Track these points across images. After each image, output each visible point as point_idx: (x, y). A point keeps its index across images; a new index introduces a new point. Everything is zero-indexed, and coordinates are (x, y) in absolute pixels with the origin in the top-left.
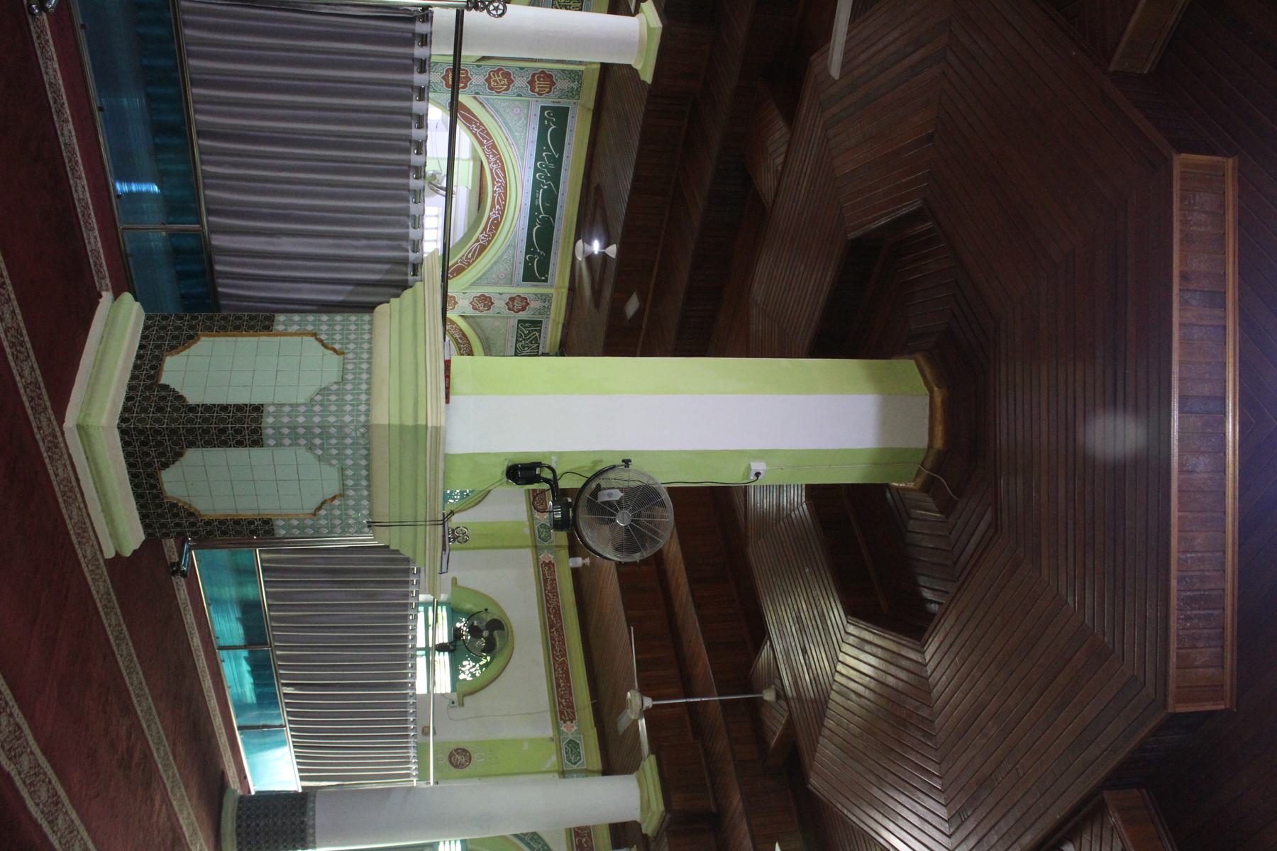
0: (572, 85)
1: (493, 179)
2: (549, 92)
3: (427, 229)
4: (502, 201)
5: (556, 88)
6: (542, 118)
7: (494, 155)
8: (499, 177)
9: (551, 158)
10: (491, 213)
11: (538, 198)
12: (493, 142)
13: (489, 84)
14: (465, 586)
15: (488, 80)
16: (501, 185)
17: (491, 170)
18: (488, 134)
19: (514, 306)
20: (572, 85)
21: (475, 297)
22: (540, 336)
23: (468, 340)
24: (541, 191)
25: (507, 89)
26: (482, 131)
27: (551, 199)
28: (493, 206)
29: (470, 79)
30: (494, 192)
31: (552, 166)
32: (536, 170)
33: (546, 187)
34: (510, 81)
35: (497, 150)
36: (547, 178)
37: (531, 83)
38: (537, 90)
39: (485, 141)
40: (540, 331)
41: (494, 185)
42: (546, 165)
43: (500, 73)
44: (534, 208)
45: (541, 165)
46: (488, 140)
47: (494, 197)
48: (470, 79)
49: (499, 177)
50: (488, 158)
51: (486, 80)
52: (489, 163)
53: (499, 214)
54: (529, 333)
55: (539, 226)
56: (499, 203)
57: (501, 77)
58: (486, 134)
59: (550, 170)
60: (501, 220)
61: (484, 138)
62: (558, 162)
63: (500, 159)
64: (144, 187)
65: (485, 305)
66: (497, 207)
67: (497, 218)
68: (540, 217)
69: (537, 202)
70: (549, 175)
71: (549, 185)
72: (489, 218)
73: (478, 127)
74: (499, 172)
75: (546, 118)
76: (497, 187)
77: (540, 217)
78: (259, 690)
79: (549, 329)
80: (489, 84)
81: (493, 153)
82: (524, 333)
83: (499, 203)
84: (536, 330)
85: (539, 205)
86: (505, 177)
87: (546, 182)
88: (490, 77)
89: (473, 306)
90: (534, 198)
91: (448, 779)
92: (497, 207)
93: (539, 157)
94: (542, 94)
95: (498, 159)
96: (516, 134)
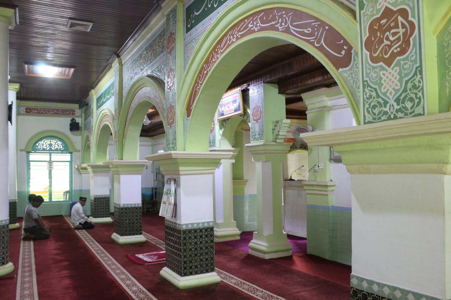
1: (229, 46)
30: (237, 39)
39: (205, 72)
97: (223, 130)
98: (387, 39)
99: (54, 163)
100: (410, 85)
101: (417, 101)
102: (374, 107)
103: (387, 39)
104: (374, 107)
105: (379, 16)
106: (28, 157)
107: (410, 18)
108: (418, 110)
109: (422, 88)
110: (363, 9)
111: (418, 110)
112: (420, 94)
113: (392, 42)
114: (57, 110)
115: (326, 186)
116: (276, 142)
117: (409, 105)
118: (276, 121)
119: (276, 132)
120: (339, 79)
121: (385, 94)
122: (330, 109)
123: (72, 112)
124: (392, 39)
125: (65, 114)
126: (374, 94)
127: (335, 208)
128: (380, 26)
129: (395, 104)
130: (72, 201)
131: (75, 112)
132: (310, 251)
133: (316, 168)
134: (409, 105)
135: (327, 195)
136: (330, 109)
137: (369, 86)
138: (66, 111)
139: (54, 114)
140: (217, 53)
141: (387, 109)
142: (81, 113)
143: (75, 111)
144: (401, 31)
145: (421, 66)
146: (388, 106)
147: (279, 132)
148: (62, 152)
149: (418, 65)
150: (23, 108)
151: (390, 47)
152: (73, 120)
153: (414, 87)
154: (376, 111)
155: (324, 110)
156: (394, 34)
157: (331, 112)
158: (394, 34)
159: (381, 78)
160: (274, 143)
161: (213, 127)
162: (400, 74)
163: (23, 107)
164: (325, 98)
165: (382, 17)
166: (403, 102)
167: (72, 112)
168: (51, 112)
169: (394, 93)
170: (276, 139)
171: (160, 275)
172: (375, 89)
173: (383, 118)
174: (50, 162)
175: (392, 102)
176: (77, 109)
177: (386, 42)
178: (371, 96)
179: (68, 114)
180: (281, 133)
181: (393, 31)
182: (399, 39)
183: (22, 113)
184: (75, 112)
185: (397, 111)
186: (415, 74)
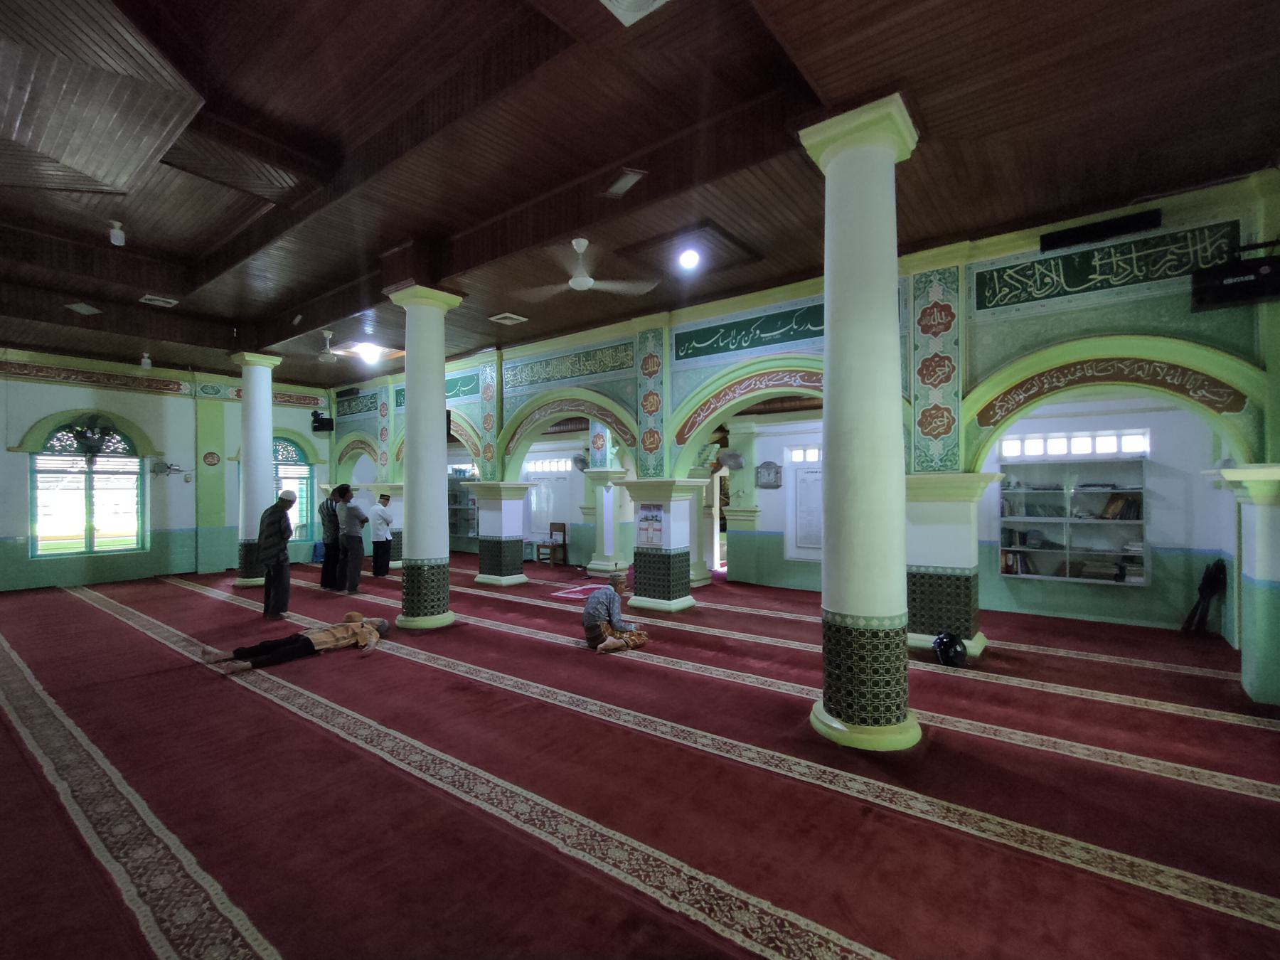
0: (650, 339)
1: (752, 390)
2: (657, 357)
3: (90, 534)
4: (778, 375)
5: (654, 352)
6: (687, 356)
7: (726, 394)
8: (750, 384)
9: (724, 337)
10: (795, 385)
11: (772, 336)
12: (712, 397)
13: (653, 411)
14: (216, 571)
15: (651, 413)
16: (759, 380)
17: (742, 394)
18: (704, 404)
19: (939, 324)
20: (650, 339)
21: (923, 382)
22: (1011, 268)
23: (1033, 378)
24: (762, 336)
25: (657, 395)
26: (702, 410)
27: (770, 323)
28: (786, 385)
29: (651, 429)
30: (767, 386)
31: (734, 333)
32: (740, 347)
33: (758, 332)
34: (651, 394)
35: (721, 392)
36: (747, 335)
37: (650, 375)
38: (656, 368)
39: (712, 406)
40: (1001, 271)
41: (759, 388)
42: (732, 339)
43: (645, 404)
44: (786, 338)
45: (733, 344)
46: (712, 404)
47: (774, 386)
48: (651, 429)
49: (750, 384)
50: (730, 400)
51: (651, 415)
52: (735, 398)
53: (795, 376)
54: (1007, 285)
55: (809, 326)
56: (782, 379)
57: (648, 403)
58: (705, 406)
59: (738, 334)
60: (801, 372)
61: (709, 408)
62: (728, 328)
63: (729, 388)
64: (1247, 278)
65: (939, 366)
66: (786, 379)
67: (802, 378)
68: (795, 327)
69: (777, 337)
70: (744, 333)
71: (755, 330)
72: (801, 386)
73: (699, 415)
74: (743, 386)
75: (686, 353)
76: (762, 384)
77: (795, 327)
78: (1269, 461)
79: (991, 258)
80: (653, 411)
81: (725, 396)
82: (1009, 293)
83: (782, 379)
84: (1000, 277)
85: (781, 334)
86: (749, 379)
87: (751, 333)
88: (648, 412)
89: (941, 382)
90: (773, 341)
91: (489, 488)
92: (786, 379)
93: (726, 349)
94: (660, 363)
95: (730, 390)
96: (703, 377)
97: (617, 448)
98: (935, 423)
99: (283, 480)
100: (950, 453)
101: (954, 462)
102: (923, 462)
103: (935, 423)
104: (923, 462)
105: (930, 408)
106: (33, 461)
107: (952, 415)
108: (956, 467)
109: (959, 455)
110: (917, 400)
111: (956, 467)
112: (957, 458)
113: (939, 426)
114: (290, 396)
115: (755, 511)
116: (703, 466)
117: (949, 464)
118: (906, 474)
119: (704, 456)
120: (706, 387)
121: (932, 455)
122: (758, 435)
123: (315, 401)
124: (939, 423)
125: (302, 403)
126: (923, 454)
127: (762, 533)
128: (931, 415)
129: (939, 462)
130: (312, 540)
131: (181, 387)
132: (728, 579)
133: (741, 493)
134: (949, 464)
135: (753, 520)
136: (758, 435)
137: (919, 449)
138: (305, 398)
139: (285, 402)
140: (734, 392)
141: (933, 464)
142: (327, 403)
143: (318, 400)
144: (946, 420)
145: (958, 443)
146: (934, 462)
147: (708, 456)
148: (296, 463)
149: (957, 442)
150: (231, 389)
151: (937, 428)
152: (315, 415)
153: (953, 454)
154: (925, 465)
155: (750, 436)
156: (941, 421)
157: (757, 438)
158: (941, 421)
159: (929, 446)
160: (701, 468)
161: (603, 444)
162: (944, 445)
163: (233, 387)
164: (753, 424)
165: (932, 409)
166: (945, 461)
167: (315, 401)
168: (279, 399)
169: (938, 455)
170: (703, 463)
171: (628, 606)
172: (924, 452)
173: (930, 469)
174: (90, 474)
175: (937, 460)
176: (322, 397)
177: (934, 425)
178: (920, 456)
179: (307, 404)
180: (710, 458)
181: (940, 419)
182: (944, 425)
183: (231, 397)
184: (181, 387)
185: (941, 466)
186: (954, 447)
